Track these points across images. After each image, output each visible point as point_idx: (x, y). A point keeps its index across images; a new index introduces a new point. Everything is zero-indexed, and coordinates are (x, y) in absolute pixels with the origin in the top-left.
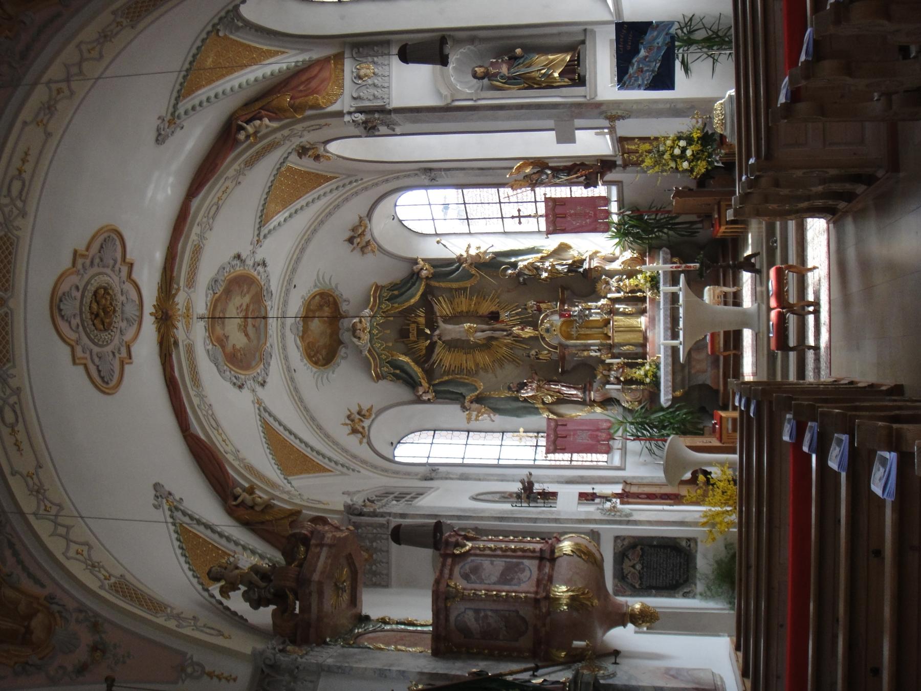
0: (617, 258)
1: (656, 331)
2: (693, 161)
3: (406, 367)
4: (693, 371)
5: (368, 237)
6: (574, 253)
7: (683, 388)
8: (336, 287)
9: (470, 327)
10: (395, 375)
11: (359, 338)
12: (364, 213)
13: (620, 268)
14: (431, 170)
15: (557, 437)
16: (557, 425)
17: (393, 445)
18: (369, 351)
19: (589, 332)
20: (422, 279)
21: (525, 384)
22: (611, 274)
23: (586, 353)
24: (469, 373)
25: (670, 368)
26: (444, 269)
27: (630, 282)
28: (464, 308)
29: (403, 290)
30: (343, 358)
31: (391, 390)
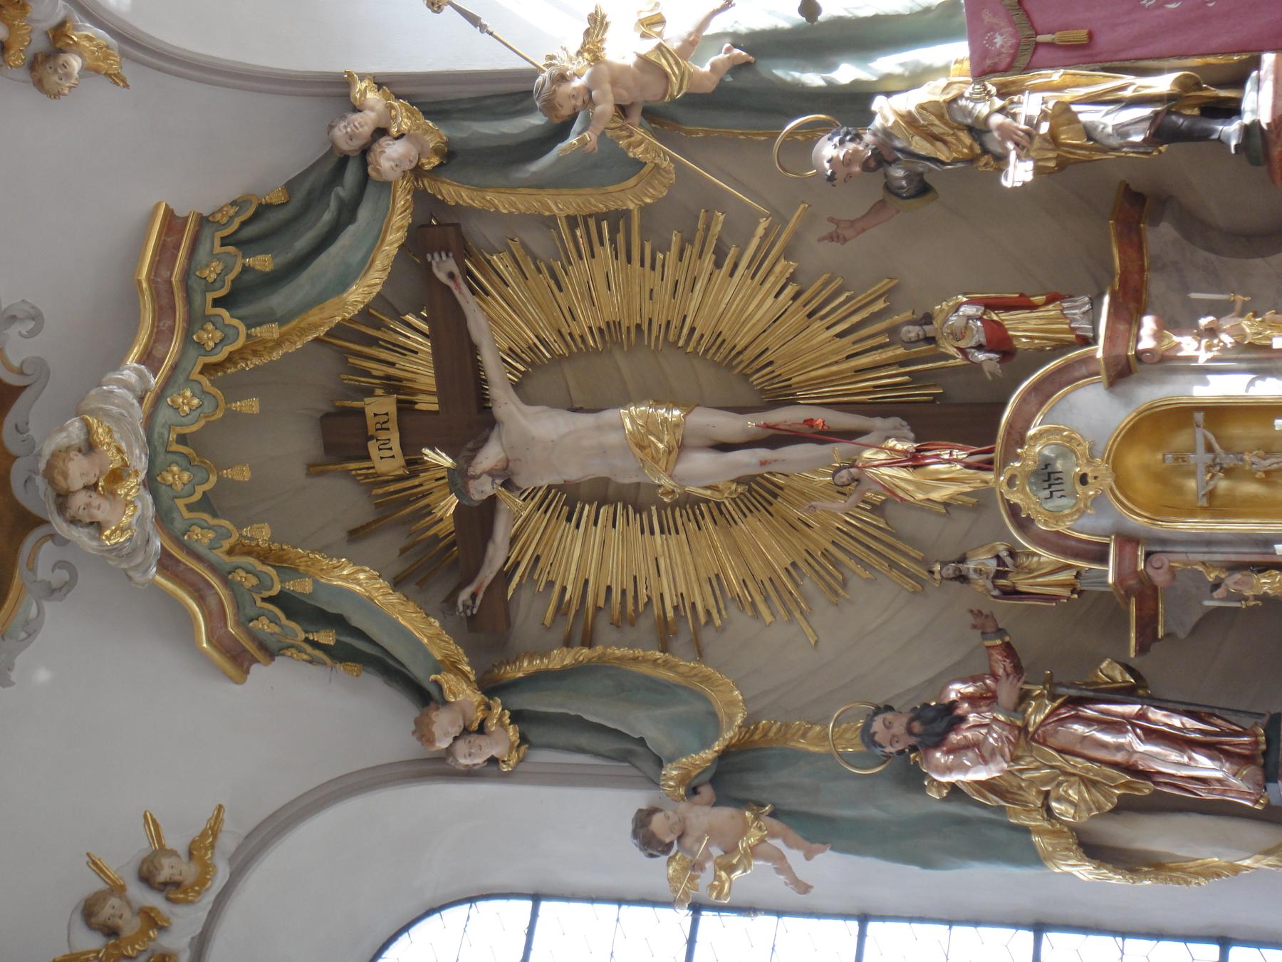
11: (98, 526)
20: (386, 186)
29: (303, 243)
30: (52, 592)
31: (309, 712)
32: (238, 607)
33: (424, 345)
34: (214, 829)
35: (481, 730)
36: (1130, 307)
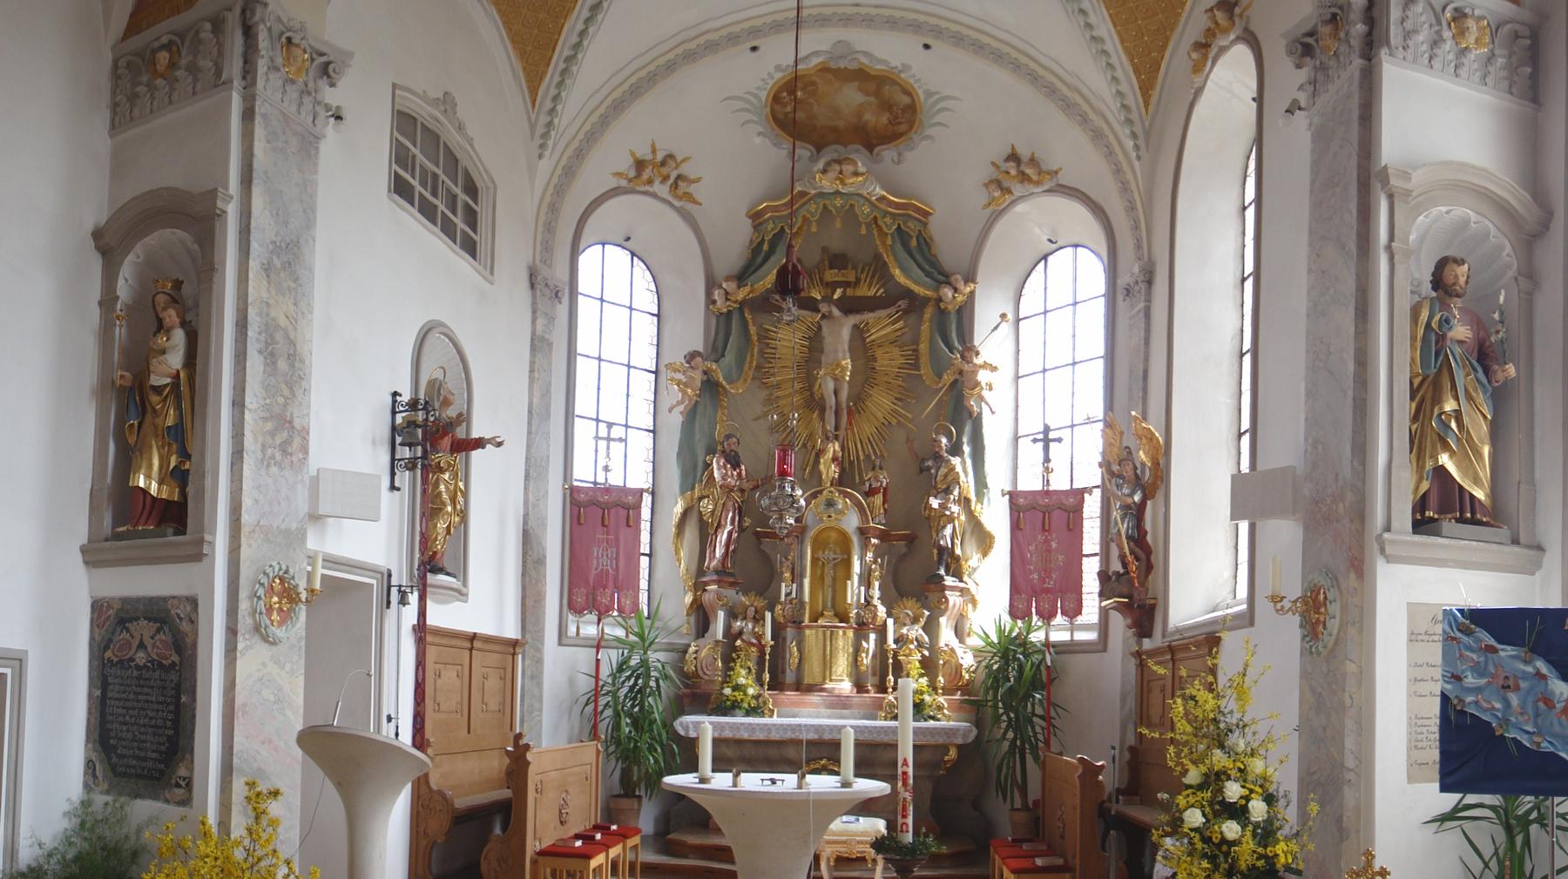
0: (962, 641)
1: (823, 711)
2: (1206, 840)
6: (973, 559)
8: (928, 137)
9: (844, 369)
10: (761, 243)
11: (824, 171)
12: (1063, 179)
13: (942, 644)
14: (1150, 282)
19: (828, 580)
20: (937, 290)
22: (931, 628)
23: (787, 575)
25: (761, 736)
26: (955, 328)
27: (913, 661)
29: (918, 257)
31: (734, 241)
33: (871, 293)
34: (695, 202)
36: (883, 536)
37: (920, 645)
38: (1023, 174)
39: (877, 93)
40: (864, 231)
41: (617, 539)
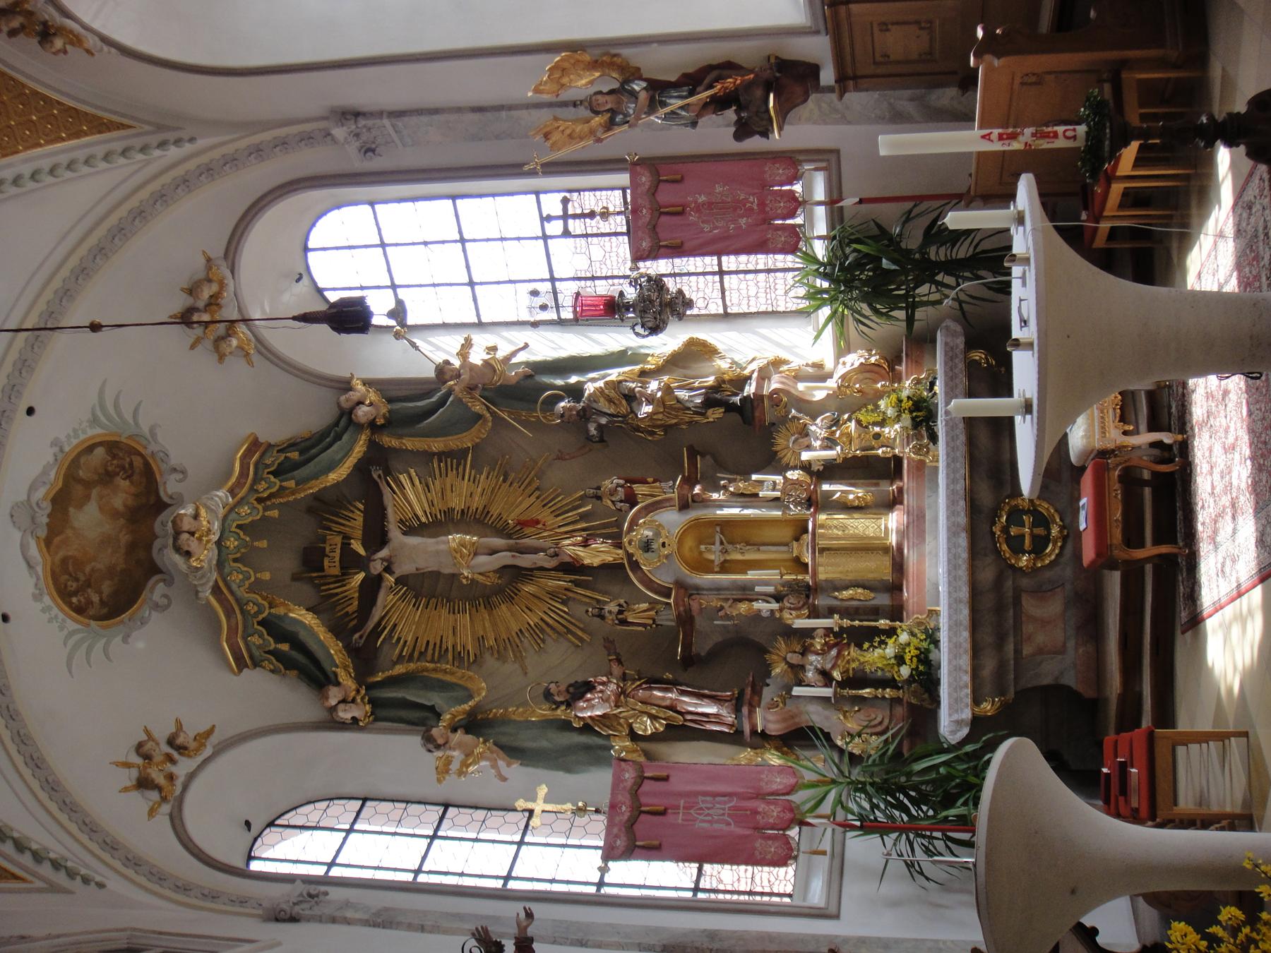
3: (303, 635)
4: (1027, 650)
5: (231, 313)
7: (1002, 692)
8: (153, 434)
9: (462, 544)
11: (188, 554)
12: (217, 251)
15: (638, 811)
16: (641, 779)
17: (253, 831)
18: (216, 590)
20: (360, 427)
21: (590, 687)
22: (813, 410)
23: (743, 607)
24: (459, 658)
25: (965, 612)
28: (457, 503)
30: (156, 607)
32: (245, 627)
34: (210, 732)
35: (353, 701)
36: (690, 481)
37: (836, 422)
38: (209, 305)
39: (88, 485)
40: (275, 513)
41: (681, 795)
